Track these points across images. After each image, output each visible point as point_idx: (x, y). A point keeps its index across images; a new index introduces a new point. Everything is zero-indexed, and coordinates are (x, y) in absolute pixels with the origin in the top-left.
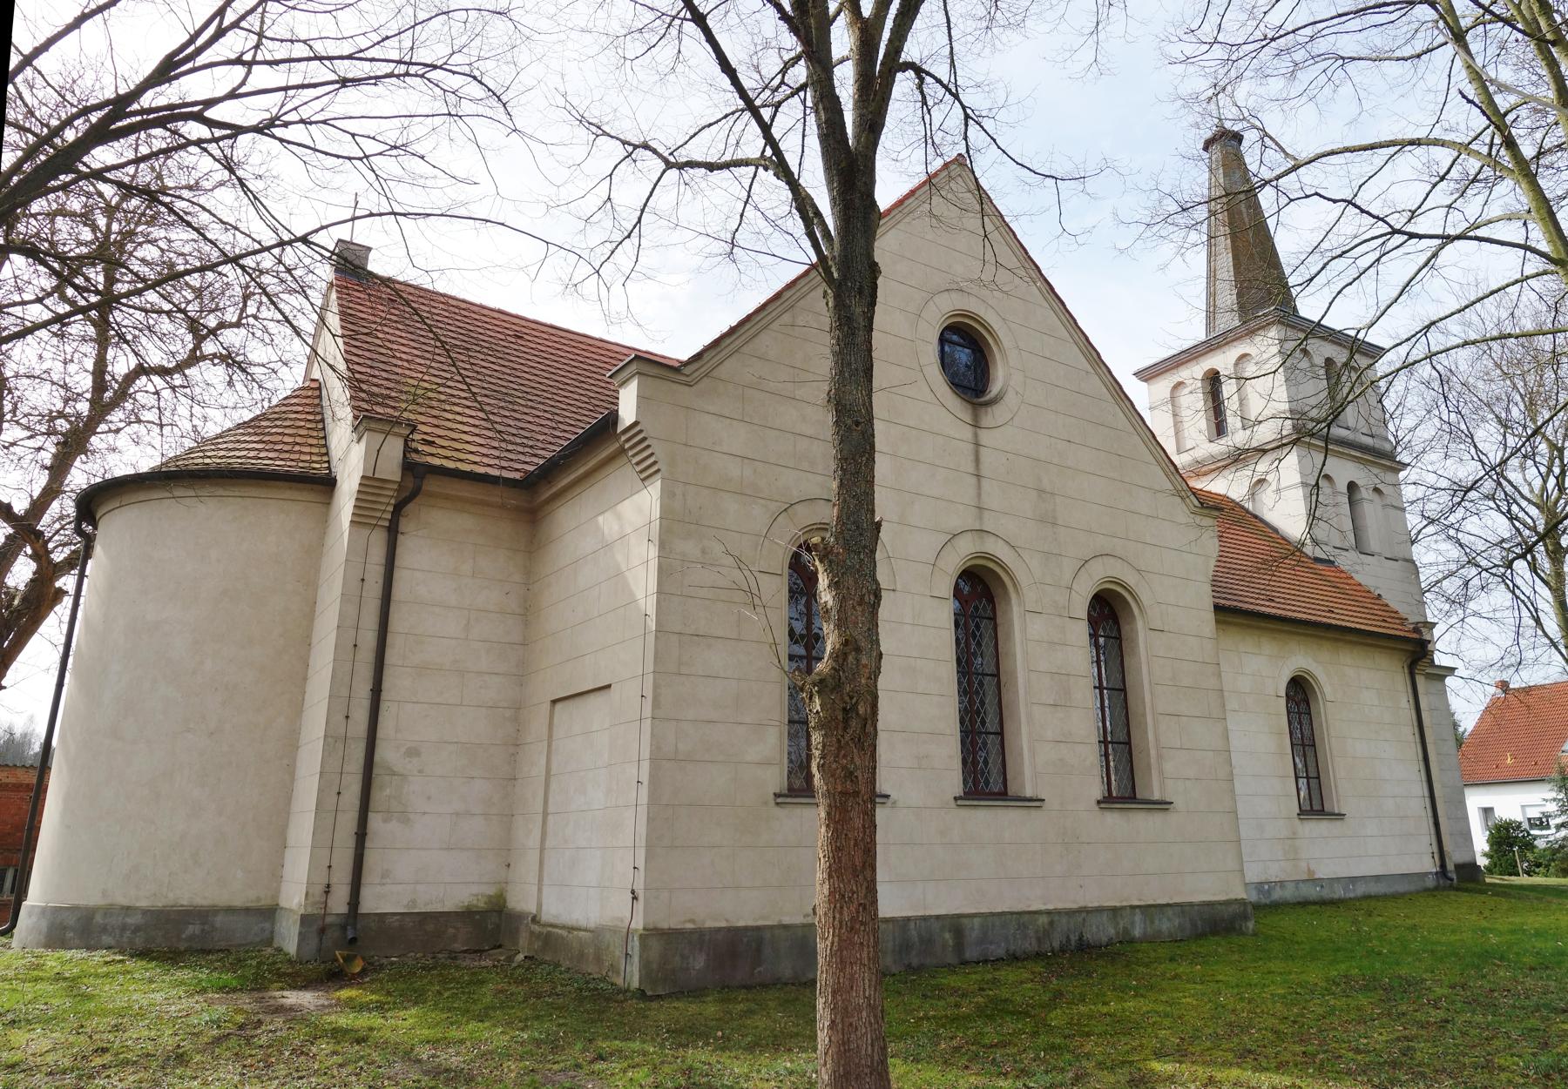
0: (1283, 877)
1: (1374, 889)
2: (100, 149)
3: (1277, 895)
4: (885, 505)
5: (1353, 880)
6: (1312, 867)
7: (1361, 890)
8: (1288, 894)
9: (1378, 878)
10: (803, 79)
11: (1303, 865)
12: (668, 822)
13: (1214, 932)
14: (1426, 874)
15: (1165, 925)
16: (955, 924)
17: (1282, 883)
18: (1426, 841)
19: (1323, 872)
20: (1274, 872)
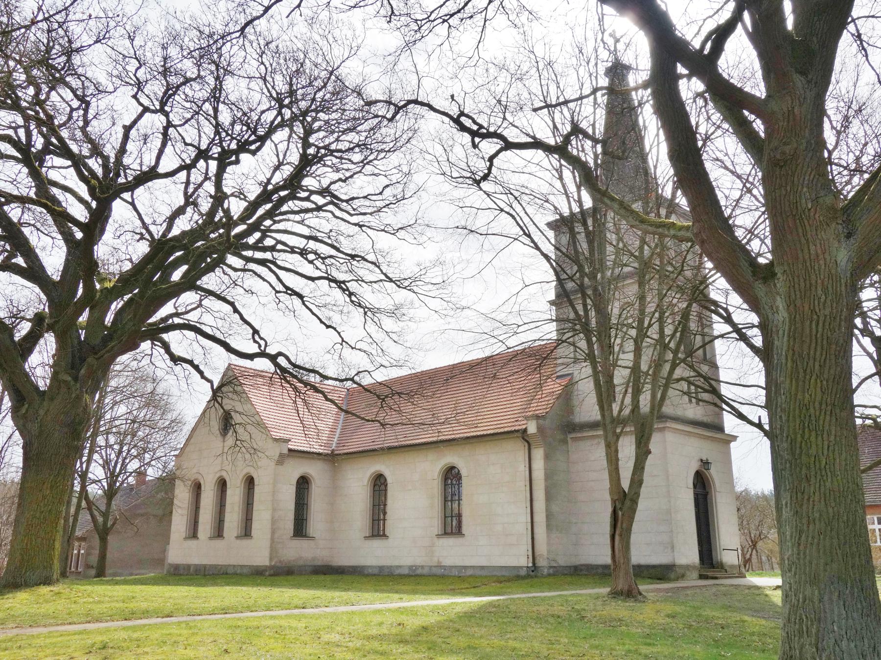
0: (424, 564)
1: (478, 572)
2: (187, 229)
3: (419, 572)
4: (203, 381)
5: (465, 567)
6: (441, 560)
7: (470, 572)
8: (425, 571)
9: (482, 568)
10: (83, 153)
11: (436, 559)
12: (775, 575)
13: (257, 574)
14: (521, 567)
15: (245, 571)
16: (205, 566)
17: (423, 567)
18: (525, 547)
19: (448, 562)
20: (419, 561)
